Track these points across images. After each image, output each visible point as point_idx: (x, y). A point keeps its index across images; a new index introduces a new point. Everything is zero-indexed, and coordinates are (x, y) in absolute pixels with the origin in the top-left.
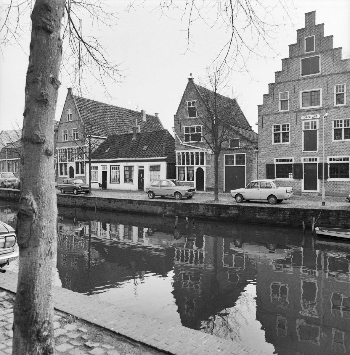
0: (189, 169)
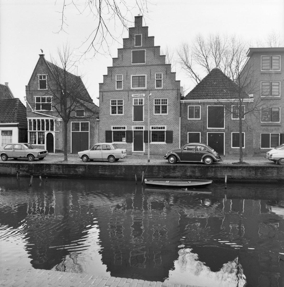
0: (31, 134)
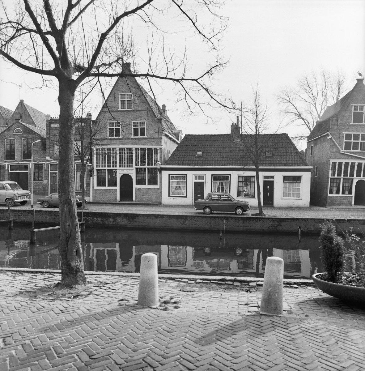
0: (345, 180)
